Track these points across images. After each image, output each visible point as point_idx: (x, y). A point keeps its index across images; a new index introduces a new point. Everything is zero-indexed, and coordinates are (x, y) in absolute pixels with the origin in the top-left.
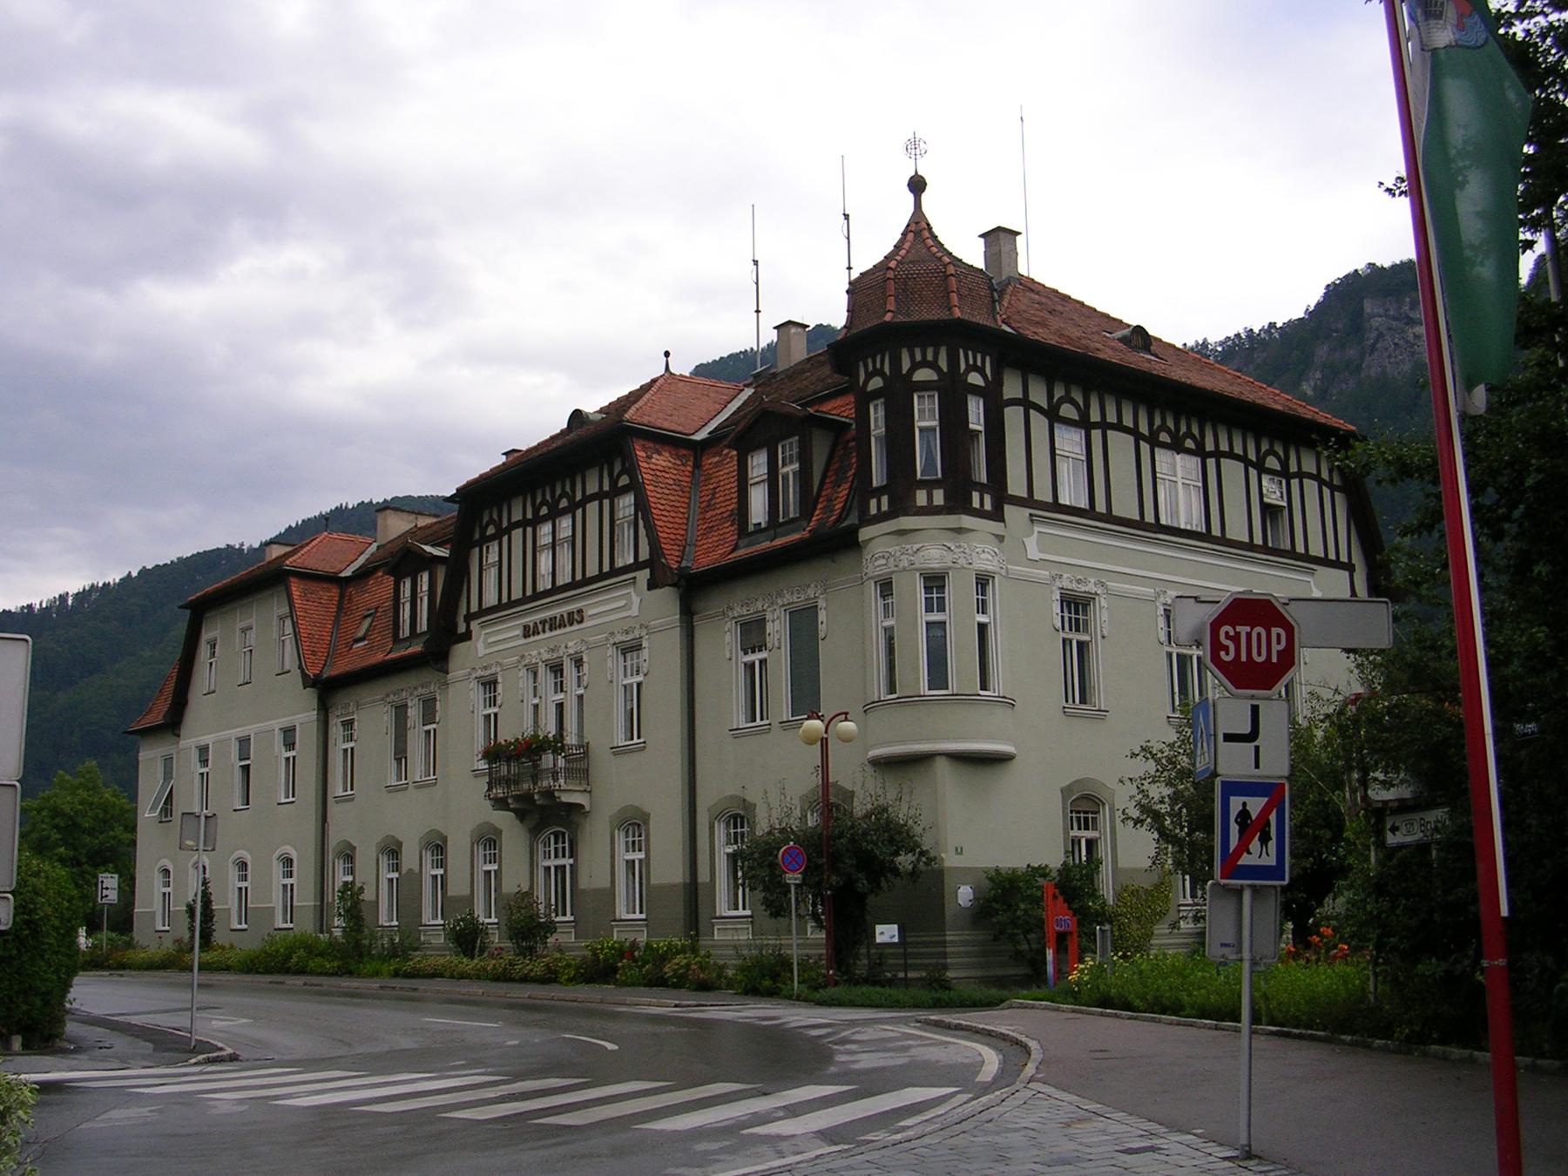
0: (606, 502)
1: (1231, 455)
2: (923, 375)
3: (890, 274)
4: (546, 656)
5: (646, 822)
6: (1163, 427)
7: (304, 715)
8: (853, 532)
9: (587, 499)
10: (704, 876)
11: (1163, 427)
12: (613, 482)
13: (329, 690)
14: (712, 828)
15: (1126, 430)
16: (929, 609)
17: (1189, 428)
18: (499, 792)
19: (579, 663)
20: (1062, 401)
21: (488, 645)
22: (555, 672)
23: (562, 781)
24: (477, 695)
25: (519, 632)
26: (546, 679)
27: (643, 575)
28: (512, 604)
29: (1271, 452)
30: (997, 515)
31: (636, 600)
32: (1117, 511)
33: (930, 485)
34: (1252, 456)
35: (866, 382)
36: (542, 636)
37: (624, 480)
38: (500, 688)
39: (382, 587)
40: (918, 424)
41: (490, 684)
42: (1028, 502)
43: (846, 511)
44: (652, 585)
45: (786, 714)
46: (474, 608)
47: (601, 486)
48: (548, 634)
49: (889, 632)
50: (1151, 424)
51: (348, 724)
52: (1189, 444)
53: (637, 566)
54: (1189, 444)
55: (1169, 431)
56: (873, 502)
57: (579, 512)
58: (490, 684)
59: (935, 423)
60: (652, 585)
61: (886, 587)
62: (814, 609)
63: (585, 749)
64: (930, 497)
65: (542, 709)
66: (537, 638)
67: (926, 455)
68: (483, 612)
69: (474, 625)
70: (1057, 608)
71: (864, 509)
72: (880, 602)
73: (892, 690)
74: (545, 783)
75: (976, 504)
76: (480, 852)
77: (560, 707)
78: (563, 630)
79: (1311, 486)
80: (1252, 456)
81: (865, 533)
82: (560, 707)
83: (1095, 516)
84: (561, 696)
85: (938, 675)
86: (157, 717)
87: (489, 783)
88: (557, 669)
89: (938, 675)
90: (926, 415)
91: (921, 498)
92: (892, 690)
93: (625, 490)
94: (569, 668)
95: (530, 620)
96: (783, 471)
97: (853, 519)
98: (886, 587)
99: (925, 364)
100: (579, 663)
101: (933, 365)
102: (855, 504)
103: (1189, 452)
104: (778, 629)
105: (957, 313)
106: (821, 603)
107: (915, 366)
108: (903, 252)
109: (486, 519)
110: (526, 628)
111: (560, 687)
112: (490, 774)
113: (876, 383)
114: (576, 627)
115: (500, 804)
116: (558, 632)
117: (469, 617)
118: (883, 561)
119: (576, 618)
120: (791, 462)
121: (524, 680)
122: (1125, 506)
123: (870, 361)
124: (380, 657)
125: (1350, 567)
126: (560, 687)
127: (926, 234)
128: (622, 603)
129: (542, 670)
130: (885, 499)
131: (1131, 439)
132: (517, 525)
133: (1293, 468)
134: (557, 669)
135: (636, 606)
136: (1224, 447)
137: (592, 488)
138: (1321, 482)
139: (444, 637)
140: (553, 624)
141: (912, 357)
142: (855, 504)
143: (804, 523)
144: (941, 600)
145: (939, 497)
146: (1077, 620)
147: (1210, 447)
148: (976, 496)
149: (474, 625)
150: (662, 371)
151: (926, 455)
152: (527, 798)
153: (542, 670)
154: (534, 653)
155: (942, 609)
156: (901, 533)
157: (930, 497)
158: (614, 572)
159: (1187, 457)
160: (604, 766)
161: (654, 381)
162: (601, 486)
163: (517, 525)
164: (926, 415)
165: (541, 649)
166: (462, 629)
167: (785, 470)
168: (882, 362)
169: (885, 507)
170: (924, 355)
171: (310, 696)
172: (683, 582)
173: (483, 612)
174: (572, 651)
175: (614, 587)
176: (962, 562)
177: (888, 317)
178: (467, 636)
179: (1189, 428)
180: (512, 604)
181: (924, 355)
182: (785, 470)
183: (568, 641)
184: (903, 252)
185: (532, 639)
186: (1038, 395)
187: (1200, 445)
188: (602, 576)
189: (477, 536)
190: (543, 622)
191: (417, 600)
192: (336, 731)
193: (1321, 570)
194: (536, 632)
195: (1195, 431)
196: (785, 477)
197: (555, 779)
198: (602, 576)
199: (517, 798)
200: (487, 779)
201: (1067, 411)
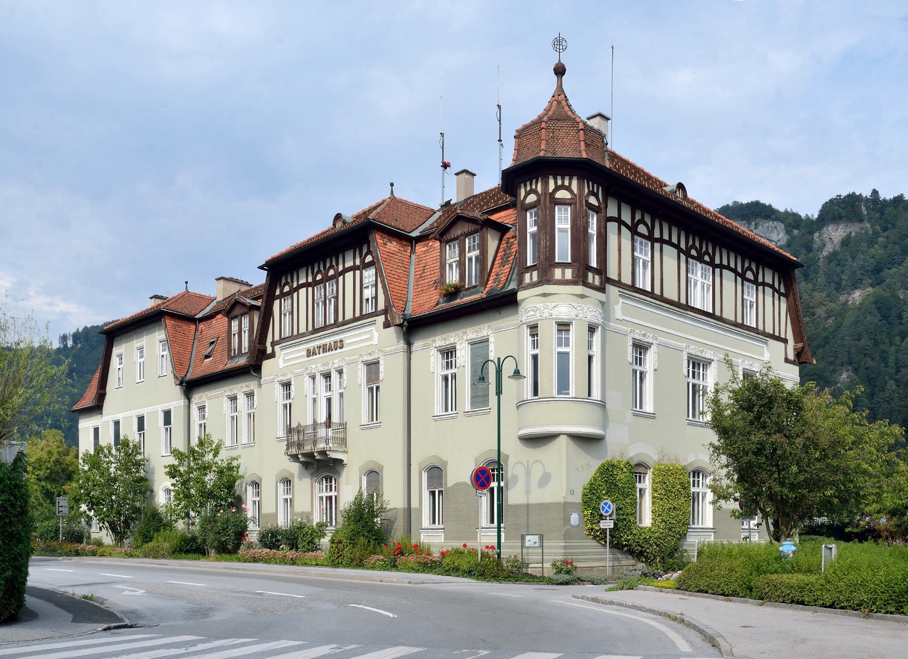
0: (358, 272)
1: (728, 268)
2: (562, 194)
3: (543, 125)
4: (321, 368)
5: (382, 471)
6: (693, 247)
7: (175, 401)
8: (514, 294)
9: (346, 270)
10: (414, 504)
11: (693, 247)
12: (363, 261)
13: (190, 387)
14: (420, 475)
15: (673, 245)
16: (560, 345)
17: (707, 248)
18: (294, 451)
19: (340, 372)
20: (639, 222)
21: (283, 362)
22: (326, 378)
23: (331, 445)
24: (279, 391)
25: (305, 353)
26: (321, 382)
27: (381, 319)
28: (300, 335)
29: (749, 269)
30: (602, 289)
31: (376, 334)
32: (666, 295)
33: (564, 265)
34: (739, 270)
35: (525, 197)
36: (318, 356)
37: (369, 259)
38: (292, 387)
39: (220, 321)
40: (557, 226)
41: (287, 385)
42: (618, 283)
43: (508, 280)
44: (387, 325)
45: (468, 407)
46: (277, 338)
47: (354, 262)
48: (322, 355)
49: (535, 358)
50: (687, 243)
51: (202, 408)
52: (707, 258)
53: (376, 314)
54: (707, 258)
55: (696, 249)
56: (527, 276)
57: (341, 278)
58: (287, 385)
59: (569, 226)
60: (387, 325)
61: (534, 328)
62: (487, 341)
63: (343, 426)
64: (563, 273)
65: (318, 401)
66: (315, 357)
67: (563, 249)
68: (282, 340)
69: (277, 348)
70: (630, 349)
71: (520, 281)
72: (530, 339)
73: (536, 393)
74: (321, 446)
75: (590, 280)
76: (281, 487)
77: (329, 400)
78: (331, 353)
79: (769, 291)
80: (739, 270)
81: (521, 295)
82: (329, 400)
83: (656, 297)
84: (330, 393)
85: (563, 386)
86: (88, 400)
87: (287, 445)
88: (327, 376)
89: (563, 386)
90: (563, 220)
91: (558, 273)
92: (536, 393)
93: (371, 264)
94: (335, 376)
95: (311, 345)
96: (468, 255)
97: (512, 286)
98: (534, 328)
99: (563, 187)
100: (340, 372)
101: (569, 189)
102: (514, 276)
103: (706, 263)
104: (463, 355)
105: (584, 156)
106: (491, 340)
107: (557, 188)
108: (550, 113)
109: (283, 282)
110: (308, 351)
111: (329, 388)
112: (288, 440)
113: (532, 198)
114: (338, 351)
115: (295, 458)
116: (328, 354)
117: (274, 344)
118: (533, 313)
119: (340, 345)
120: (474, 250)
121: (308, 381)
122: (671, 293)
123: (528, 183)
124: (220, 368)
125: (785, 341)
126: (329, 388)
127: (564, 103)
128: (368, 336)
129: (318, 377)
130: (535, 274)
131: (676, 251)
132: (302, 286)
133: (760, 280)
134: (327, 376)
135: (377, 339)
136: (725, 263)
137: (349, 264)
138: (774, 290)
139: (259, 356)
140: (325, 349)
141: (556, 183)
142: (514, 276)
143: (482, 289)
144: (567, 339)
145: (569, 274)
146: (640, 359)
147: (717, 261)
148: (590, 275)
149: (277, 348)
150: (389, 195)
151: (563, 249)
152: (310, 455)
153: (318, 377)
154: (313, 366)
155: (567, 345)
156: (545, 295)
157: (563, 273)
158: (362, 317)
159: (704, 266)
160: (353, 434)
161: (384, 201)
162: (354, 262)
163: (302, 286)
164: (563, 220)
165: (318, 364)
166: (269, 350)
167: (470, 254)
168: (536, 186)
169: (535, 279)
170: (563, 182)
171: (177, 391)
172: (405, 323)
173: (282, 340)
174: (336, 366)
175: (363, 326)
176: (581, 316)
177: (542, 154)
178: (273, 355)
179: (707, 248)
180: (300, 335)
181: (563, 182)
182: (470, 254)
183: (333, 360)
184: (550, 113)
185: (312, 358)
186: (626, 217)
187: (712, 259)
188: (355, 319)
189: (278, 292)
190: (319, 347)
191: (242, 330)
192: (195, 412)
193: (771, 342)
194: (314, 354)
195: (710, 251)
196: (470, 259)
197: (327, 443)
198: (355, 319)
199: (304, 455)
200: (286, 443)
201: (642, 229)
